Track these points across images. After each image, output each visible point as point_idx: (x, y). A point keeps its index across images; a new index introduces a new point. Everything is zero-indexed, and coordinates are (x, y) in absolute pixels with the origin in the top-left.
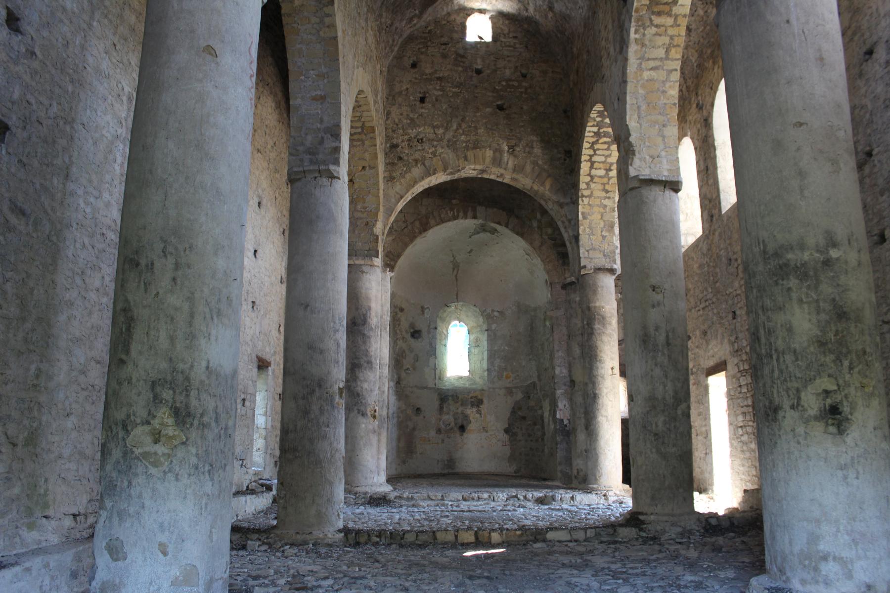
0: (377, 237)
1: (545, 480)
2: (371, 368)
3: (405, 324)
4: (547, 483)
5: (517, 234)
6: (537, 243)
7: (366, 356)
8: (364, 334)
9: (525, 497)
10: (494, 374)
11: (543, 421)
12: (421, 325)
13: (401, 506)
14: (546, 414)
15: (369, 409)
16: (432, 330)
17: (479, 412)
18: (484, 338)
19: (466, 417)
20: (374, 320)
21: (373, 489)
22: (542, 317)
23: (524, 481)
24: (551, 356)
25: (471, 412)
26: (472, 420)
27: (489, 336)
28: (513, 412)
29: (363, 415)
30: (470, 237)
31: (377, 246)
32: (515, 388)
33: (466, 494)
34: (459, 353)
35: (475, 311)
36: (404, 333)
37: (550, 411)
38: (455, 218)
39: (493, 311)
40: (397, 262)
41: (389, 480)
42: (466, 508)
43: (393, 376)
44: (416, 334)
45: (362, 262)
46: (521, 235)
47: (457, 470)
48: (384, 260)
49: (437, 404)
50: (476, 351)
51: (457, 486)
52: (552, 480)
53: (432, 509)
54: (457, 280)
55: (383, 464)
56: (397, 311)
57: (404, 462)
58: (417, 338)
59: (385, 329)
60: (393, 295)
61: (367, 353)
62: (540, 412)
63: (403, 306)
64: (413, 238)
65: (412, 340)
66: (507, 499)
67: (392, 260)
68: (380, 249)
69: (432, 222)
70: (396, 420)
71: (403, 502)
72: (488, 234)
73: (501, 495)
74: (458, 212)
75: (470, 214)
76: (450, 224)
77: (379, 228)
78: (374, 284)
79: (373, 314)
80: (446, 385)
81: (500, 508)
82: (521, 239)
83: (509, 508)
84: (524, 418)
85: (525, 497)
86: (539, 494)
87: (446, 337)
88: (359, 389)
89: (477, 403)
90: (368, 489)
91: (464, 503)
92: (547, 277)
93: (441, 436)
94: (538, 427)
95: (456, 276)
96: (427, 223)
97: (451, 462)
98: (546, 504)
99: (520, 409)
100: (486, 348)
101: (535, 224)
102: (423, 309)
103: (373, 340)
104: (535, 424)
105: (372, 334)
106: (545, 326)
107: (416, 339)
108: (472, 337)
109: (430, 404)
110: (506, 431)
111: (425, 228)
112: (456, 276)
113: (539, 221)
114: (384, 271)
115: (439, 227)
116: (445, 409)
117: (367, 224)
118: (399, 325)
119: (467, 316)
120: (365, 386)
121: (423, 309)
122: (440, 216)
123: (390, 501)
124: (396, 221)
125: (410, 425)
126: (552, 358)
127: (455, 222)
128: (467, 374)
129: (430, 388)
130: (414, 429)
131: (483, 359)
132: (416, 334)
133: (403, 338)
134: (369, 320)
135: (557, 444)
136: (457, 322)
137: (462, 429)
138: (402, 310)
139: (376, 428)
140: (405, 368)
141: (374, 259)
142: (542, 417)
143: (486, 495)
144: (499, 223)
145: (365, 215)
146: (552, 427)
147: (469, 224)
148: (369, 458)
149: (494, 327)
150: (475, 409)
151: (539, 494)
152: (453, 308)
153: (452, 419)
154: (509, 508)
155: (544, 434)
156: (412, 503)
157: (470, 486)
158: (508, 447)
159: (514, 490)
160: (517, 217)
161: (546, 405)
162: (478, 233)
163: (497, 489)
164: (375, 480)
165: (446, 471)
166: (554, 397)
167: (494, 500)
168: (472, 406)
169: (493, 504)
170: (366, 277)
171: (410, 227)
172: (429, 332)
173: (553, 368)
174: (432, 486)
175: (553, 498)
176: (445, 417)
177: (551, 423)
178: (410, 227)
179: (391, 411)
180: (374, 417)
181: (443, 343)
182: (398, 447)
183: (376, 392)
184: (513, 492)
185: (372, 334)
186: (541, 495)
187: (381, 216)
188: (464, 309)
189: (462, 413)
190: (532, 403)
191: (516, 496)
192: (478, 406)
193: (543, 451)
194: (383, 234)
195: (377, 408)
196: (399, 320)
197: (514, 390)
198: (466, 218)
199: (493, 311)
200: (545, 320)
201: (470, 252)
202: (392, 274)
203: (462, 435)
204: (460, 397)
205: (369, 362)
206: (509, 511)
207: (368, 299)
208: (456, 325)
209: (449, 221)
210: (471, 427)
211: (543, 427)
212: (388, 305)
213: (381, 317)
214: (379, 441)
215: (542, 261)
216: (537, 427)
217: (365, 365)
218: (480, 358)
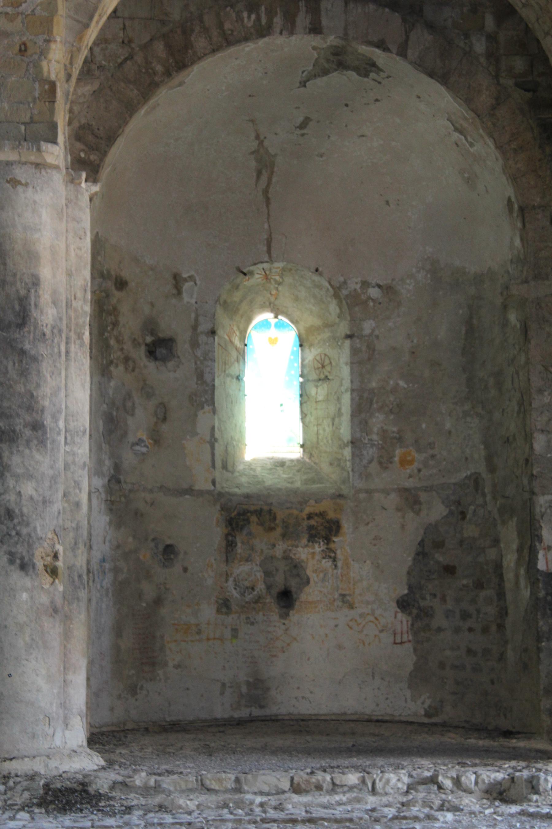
0: (53, 85)
1: (508, 734)
2: (42, 443)
3: (130, 323)
4: (514, 743)
5: (431, 75)
6: (485, 99)
7: (30, 409)
8: (23, 352)
9: (457, 782)
10: (370, 452)
11: (501, 576)
12: (173, 325)
13: (129, 810)
14: (510, 559)
15: (39, 552)
16: (202, 339)
17: (330, 555)
18: (342, 357)
19: (296, 568)
20: (47, 315)
21: (53, 764)
22: (499, 301)
23: (451, 738)
24: (521, 404)
25: (308, 554)
26: (313, 577)
27: (354, 351)
28: (422, 554)
29: (23, 567)
30: (303, 84)
31: (52, 111)
32: (426, 489)
33: (301, 776)
34: (273, 403)
35: (319, 287)
36: (128, 346)
37: (520, 550)
38: (263, 31)
39: (365, 284)
40: (105, 154)
41: (96, 740)
42: (301, 814)
43: (100, 462)
44: (160, 348)
45: (12, 156)
46: (443, 79)
47: (272, 710)
48: (71, 150)
49: (218, 534)
50: (319, 392)
51: (275, 752)
52: (529, 734)
53: (211, 815)
54: (268, 201)
55: (79, 696)
56: (109, 286)
57: (133, 690)
58: (164, 360)
59: (80, 336)
60: (98, 246)
61: (31, 404)
62: (492, 554)
63: (125, 274)
64: (148, 87)
65: (151, 365)
66: (410, 788)
67: (92, 148)
68: (61, 119)
69: (200, 43)
70: (109, 577)
71: (134, 799)
72: (352, 74)
73: (393, 777)
74: (271, 14)
75: (303, 19)
76: (249, 47)
77: (57, 60)
78: (46, 216)
79: (45, 297)
80: (240, 485)
81: (391, 812)
82: (443, 89)
83: (415, 810)
84: (450, 570)
85: (457, 782)
86: (494, 774)
87: (241, 355)
88: (12, 497)
89: (325, 529)
90: (38, 766)
91: (296, 798)
92: (510, 192)
93: (230, 619)
94: (488, 592)
95: (266, 192)
96: (188, 46)
97: (257, 689)
98: (513, 802)
99: (439, 545)
100: (347, 383)
101: (480, 46)
102: (177, 281)
103: (46, 367)
104: (479, 585)
105: (42, 349)
106: (505, 324)
107: (164, 361)
108: (312, 354)
109: (200, 533)
110: (403, 604)
111: (180, 59)
112: (266, 192)
113: (492, 38)
114: (72, 181)
115: (219, 55)
116: (240, 549)
117: (23, 49)
118: (115, 324)
119: (297, 299)
120: (28, 489)
121: (177, 281)
122: (220, 25)
123: (99, 796)
124: (101, 40)
125: (149, 591)
126: (524, 408)
127: (262, 42)
128: (296, 453)
129: (201, 493)
130: (158, 601)
131: (339, 413)
132: (160, 348)
133: (127, 359)
134: (34, 313)
135: (539, 639)
136: (268, 316)
137: (286, 598)
138: (121, 284)
139: (59, 601)
140: (131, 438)
141: (46, 146)
142: (498, 567)
143: (353, 778)
144: (381, 45)
145: (18, 24)
146: (526, 593)
147: (298, 46)
148: (41, 682)
149: (368, 326)
150: (319, 548)
151: (494, 774)
152: (257, 278)
153: (260, 575)
154: (415, 810)
155: (503, 612)
156: (159, 799)
157: (309, 752)
158: (409, 647)
159: (425, 762)
160: (431, 27)
161: (510, 535)
162: (325, 72)
163: (380, 761)
164: (58, 741)
165: (244, 713)
166: (531, 514)
167: (374, 791)
168: (313, 537)
169: (372, 801)
170: (23, 196)
171: (139, 58)
172: (195, 344)
173: (528, 438)
174: (210, 752)
175: (533, 786)
176: (241, 569)
177: (522, 582)
178: (139, 58)
179: (97, 555)
180: (53, 572)
181: (234, 370)
182: (116, 648)
183: (58, 505)
184: (426, 767)
185: (42, 349)
186: (500, 776)
187: (61, 29)
188: (288, 280)
189: (286, 558)
190: (471, 531)
191: (433, 780)
192: (328, 540)
193: (502, 657)
194: (69, 77)
195: (60, 548)
196: (115, 311)
197: (423, 496)
198: (292, 33)
199: (365, 284)
200: (505, 307)
201: (303, 125)
202: (96, 188)
203: (285, 616)
204: (280, 515)
205: (37, 426)
206: (416, 819)
207: (32, 256)
208: (266, 324)
209: (246, 39)
210: (311, 594)
211: (501, 594)
212: (87, 273)
213: (68, 305)
214: (67, 635)
215: (499, 147)
216: (484, 594)
217: (28, 432)
218: (332, 409)
